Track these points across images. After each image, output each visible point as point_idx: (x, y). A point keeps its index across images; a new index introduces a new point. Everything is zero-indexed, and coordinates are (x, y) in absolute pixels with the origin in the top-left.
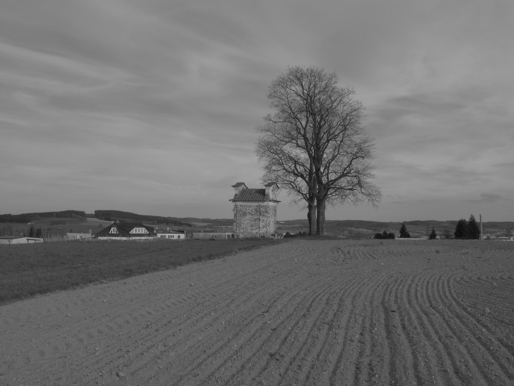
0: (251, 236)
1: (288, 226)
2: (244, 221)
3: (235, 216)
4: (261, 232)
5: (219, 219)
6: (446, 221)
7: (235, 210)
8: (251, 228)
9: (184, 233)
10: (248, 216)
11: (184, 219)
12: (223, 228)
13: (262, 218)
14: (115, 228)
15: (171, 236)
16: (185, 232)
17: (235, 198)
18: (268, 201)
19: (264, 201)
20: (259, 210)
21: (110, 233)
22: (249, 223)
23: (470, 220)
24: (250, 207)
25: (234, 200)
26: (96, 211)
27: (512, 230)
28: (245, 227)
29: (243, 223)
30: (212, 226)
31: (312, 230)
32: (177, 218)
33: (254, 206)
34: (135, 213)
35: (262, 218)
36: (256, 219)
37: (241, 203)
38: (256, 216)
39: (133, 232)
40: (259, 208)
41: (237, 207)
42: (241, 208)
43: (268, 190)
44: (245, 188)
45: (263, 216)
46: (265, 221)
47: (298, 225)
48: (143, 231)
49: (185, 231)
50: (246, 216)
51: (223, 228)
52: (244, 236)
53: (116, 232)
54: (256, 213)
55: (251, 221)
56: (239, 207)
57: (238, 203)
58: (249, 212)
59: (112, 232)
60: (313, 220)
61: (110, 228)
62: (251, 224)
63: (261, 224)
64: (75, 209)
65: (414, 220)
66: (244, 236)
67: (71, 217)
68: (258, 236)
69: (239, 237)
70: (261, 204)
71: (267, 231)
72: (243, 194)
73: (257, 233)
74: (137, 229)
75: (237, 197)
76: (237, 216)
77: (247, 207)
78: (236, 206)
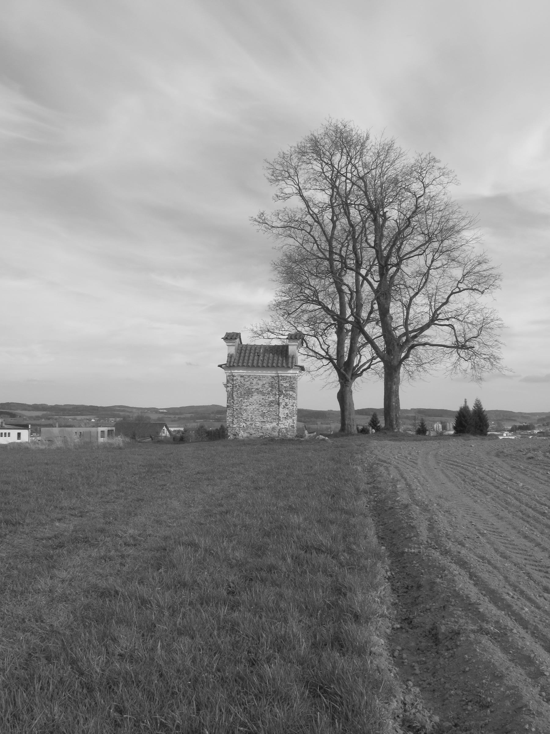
0: (262, 434)
1: (172, 416)
2: (247, 406)
3: (230, 396)
4: (282, 426)
6: (411, 409)
7: (228, 385)
8: (261, 418)
9: (28, 429)
10: (256, 397)
12: (69, 419)
13: (283, 400)
15: (5, 433)
16: (30, 427)
17: (229, 361)
18: (296, 368)
19: (289, 368)
22: (258, 410)
23: (474, 407)
27: (503, 423)
28: (250, 417)
29: (246, 410)
31: (346, 422)
33: (267, 378)
35: (283, 400)
36: (272, 402)
40: (277, 381)
41: (233, 380)
47: (189, 415)
49: (30, 425)
50: (252, 396)
51: (69, 419)
52: (249, 435)
54: (271, 390)
56: (237, 379)
57: (236, 371)
58: (257, 389)
60: (348, 404)
65: (365, 408)
66: (249, 435)
68: (276, 434)
70: (282, 373)
71: (292, 424)
72: (242, 355)
73: (273, 428)
75: (233, 360)
76: (234, 396)
77: (253, 380)
78: (231, 379)
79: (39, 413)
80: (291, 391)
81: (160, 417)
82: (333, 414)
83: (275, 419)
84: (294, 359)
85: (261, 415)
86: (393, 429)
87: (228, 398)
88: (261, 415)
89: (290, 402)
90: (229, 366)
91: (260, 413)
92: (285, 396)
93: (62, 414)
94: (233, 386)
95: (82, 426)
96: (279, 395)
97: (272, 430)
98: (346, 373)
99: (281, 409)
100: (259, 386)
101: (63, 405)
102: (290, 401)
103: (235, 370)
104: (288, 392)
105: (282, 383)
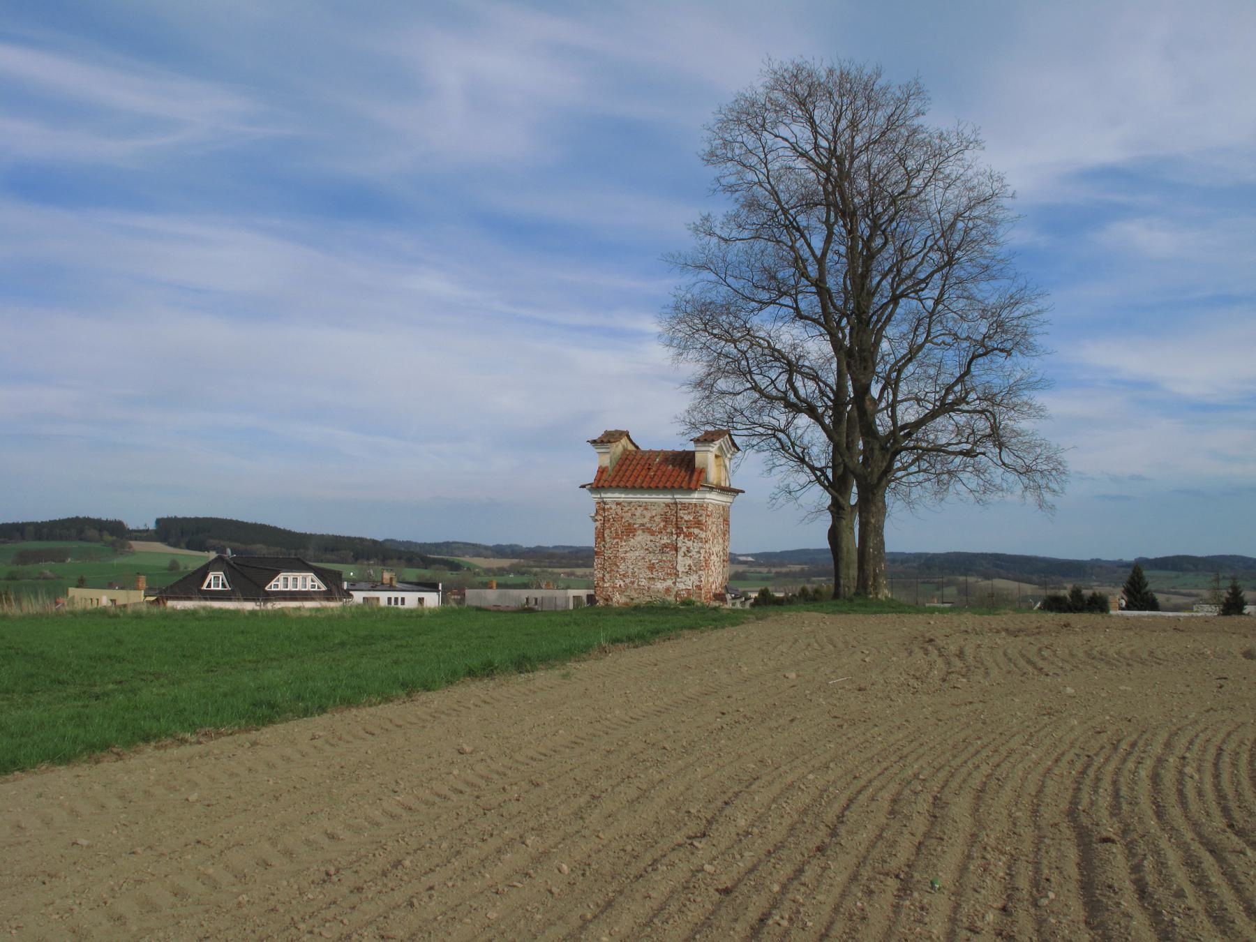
1: (765, 570)
2: (626, 552)
3: (600, 535)
4: (682, 586)
5: (548, 548)
7: (599, 517)
9: (438, 591)
10: (641, 538)
11: (437, 545)
14: (221, 574)
16: (440, 588)
17: (598, 479)
19: (690, 490)
20: (675, 520)
21: (204, 588)
22: (643, 558)
24: (646, 509)
25: (596, 487)
26: (158, 521)
29: (623, 559)
30: (524, 569)
31: (842, 582)
32: (416, 544)
34: (281, 526)
35: (683, 543)
36: (665, 546)
37: (617, 495)
38: (665, 538)
39: (277, 586)
40: (674, 512)
41: (604, 509)
42: (619, 512)
43: (704, 454)
44: (631, 447)
45: (689, 535)
46: (694, 553)
47: (797, 568)
48: (309, 583)
49: (440, 585)
52: (628, 600)
53: (224, 585)
54: (665, 526)
55: (650, 553)
56: (611, 508)
57: (609, 495)
59: (209, 585)
60: (845, 549)
61: (203, 573)
62: (650, 561)
63: (682, 563)
64: (94, 515)
66: (628, 600)
67: (81, 539)
68: (671, 599)
69: (610, 603)
70: (680, 498)
71: (698, 584)
72: (624, 468)
73: (668, 590)
74: (291, 576)
76: (606, 535)
77: (636, 509)
78: (602, 507)
79: (505, 563)
80: (697, 527)
81: (740, 570)
82: (1101, 567)
83: (671, 574)
84: (703, 475)
85: (648, 568)
86: (867, 594)
87: (596, 539)
88: (648, 568)
89: (694, 546)
90: (597, 486)
91: (647, 564)
92: (687, 536)
93: (547, 564)
94: (606, 520)
95: (543, 586)
96: (676, 534)
97: (666, 593)
98: (840, 495)
99: (679, 557)
100: (646, 520)
101: (551, 546)
102: (695, 544)
103: (606, 493)
104: (691, 530)
105: (682, 515)
